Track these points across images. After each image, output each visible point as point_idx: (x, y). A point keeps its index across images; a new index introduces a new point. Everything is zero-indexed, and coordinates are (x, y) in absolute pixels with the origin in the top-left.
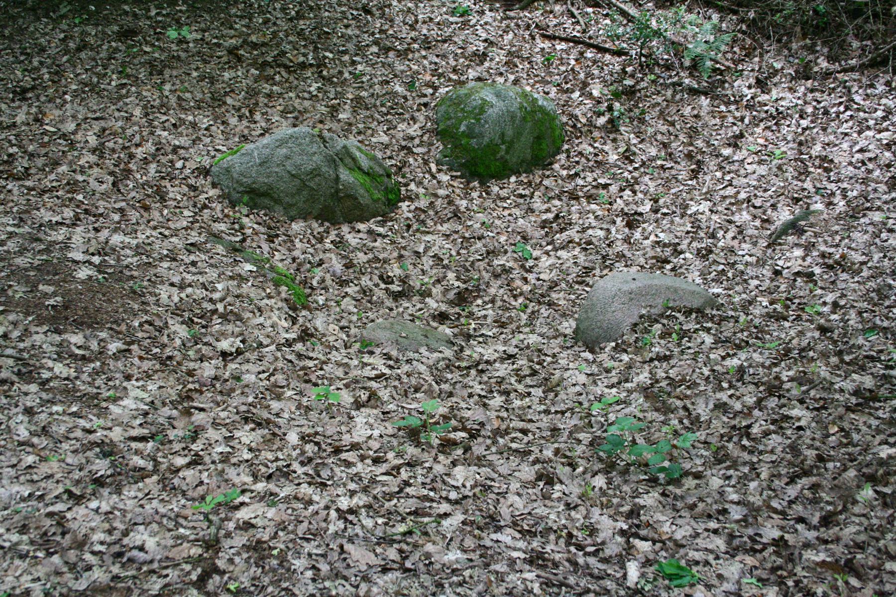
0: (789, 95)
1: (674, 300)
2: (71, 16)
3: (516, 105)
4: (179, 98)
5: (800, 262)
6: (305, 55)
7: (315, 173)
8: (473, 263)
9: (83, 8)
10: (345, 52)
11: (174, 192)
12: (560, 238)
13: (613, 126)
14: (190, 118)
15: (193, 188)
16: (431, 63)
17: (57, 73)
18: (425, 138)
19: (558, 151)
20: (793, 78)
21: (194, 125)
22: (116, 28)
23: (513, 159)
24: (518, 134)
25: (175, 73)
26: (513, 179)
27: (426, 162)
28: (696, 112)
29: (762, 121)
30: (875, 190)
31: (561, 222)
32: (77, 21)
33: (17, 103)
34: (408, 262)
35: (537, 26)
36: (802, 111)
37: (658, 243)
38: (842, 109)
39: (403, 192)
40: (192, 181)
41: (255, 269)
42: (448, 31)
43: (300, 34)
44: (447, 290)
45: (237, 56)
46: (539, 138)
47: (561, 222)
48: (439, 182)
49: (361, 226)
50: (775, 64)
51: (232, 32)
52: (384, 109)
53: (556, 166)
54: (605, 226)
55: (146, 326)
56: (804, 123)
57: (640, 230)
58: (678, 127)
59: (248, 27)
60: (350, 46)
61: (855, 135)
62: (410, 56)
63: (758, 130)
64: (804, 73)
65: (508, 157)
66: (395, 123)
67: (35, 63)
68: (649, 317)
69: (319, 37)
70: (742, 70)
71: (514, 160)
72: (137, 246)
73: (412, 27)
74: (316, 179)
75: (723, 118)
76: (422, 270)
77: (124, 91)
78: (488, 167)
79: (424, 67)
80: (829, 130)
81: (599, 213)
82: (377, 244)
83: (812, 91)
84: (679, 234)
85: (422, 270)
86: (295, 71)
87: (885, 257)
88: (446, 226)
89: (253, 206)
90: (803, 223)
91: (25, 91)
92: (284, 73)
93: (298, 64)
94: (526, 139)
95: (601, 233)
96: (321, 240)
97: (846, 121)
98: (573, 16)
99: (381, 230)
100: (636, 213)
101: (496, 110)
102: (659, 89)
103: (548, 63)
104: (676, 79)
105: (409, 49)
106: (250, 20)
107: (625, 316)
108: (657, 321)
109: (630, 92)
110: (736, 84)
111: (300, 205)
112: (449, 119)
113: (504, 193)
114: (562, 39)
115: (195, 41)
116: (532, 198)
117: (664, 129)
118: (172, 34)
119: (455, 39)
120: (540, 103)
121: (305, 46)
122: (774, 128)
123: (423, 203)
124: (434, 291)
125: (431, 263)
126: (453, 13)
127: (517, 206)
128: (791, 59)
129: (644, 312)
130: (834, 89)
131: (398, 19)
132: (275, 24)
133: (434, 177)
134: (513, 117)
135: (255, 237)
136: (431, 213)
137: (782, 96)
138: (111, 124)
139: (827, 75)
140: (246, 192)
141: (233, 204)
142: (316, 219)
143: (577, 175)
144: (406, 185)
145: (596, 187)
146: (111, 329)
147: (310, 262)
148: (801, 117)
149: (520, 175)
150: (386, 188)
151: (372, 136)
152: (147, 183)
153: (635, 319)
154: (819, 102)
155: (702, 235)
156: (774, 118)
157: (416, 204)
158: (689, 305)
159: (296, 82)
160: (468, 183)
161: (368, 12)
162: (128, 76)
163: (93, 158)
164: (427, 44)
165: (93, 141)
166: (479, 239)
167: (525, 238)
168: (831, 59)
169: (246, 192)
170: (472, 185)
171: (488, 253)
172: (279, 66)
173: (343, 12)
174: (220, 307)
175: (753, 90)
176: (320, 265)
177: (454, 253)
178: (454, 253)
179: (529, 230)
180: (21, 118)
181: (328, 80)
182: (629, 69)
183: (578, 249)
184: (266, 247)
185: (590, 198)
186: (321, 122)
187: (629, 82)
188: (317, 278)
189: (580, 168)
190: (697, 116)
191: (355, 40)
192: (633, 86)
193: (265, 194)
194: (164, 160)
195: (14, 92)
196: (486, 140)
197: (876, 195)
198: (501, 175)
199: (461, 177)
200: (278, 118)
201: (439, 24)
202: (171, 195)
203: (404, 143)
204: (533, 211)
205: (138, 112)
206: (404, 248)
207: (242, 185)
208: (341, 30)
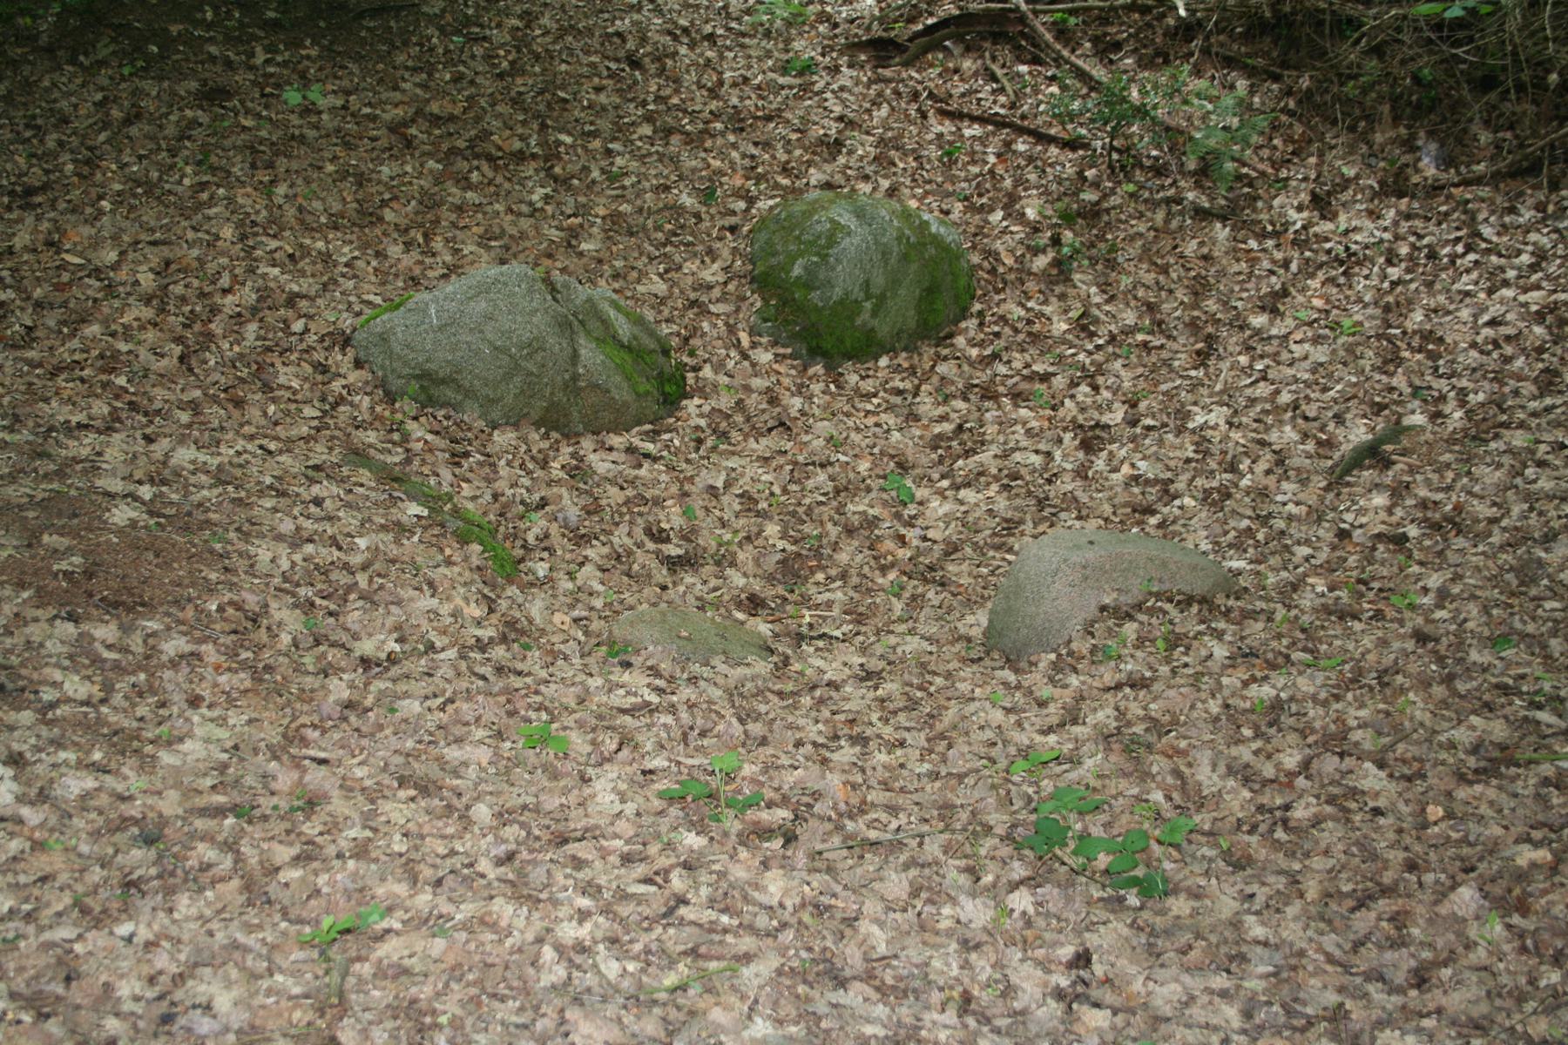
0: (1368, 224)
3: (892, 233)
6: (522, 138)
7: (534, 347)
8: (810, 508)
10: (594, 134)
11: (287, 376)
14: (320, 245)
17: (88, 162)
18: (731, 287)
19: (964, 314)
20: (1375, 195)
22: (193, 85)
23: (883, 329)
24: (894, 282)
25: (295, 165)
26: (884, 361)
27: (731, 329)
28: (1205, 250)
29: (1320, 266)
32: (126, 71)
35: (931, 95)
38: (1460, 249)
40: (319, 356)
42: (776, 102)
45: (404, 136)
46: (931, 291)
49: (616, 440)
50: (1345, 170)
53: (960, 341)
54: (1042, 447)
56: (1394, 273)
58: (1174, 275)
59: (424, 86)
60: (604, 124)
61: (1482, 295)
62: (709, 144)
63: (1314, 284)
64: (1395, 186)
70: (1287, 179)
72: (220, 467)
75: (1253, 262)
79: (732, 163)
80: (1438, 286)
81: (1034, 424)
84: (1172, 464)
87: (1531, 509)
88: (764, 441)
90: (1389, 448)
91: (30, 191)
92: (485, 167)
95: (1036, 460)
97: (1468, 271)
98: (994, 78)
101: (856, 240)
102: (1142, 208)
103: (949, 160)
104: (1172, 191)
105: (706, 131)
109: (1093, 214)
110: (1276, 203)
113: (868, 386)
114: (973, 119)
117: (1149, 278)
119: (788, 115)
120: (933, 229)
121: (524, 123)
122: (1342, 280)
123: (725, 402)
125: (738, 508)
126: (784, 71)
129: (1107, 600)
130: (1446, 214)
132: (472, 82)
136: (739, 418)
137: (1357, 225)
139: (1436, 189)
140: (418, 377)
142: (537, 425)
143: (995, 356)
144: (696, 369)
145: (1029, 378)
148: (1389, 262)
150: (661, 374)
156: (1342, 263)
158: (1187, 589)
161: (635, 64)
163: (148, 313)
164: (738, 122)
165: (147, 280)
166: (822, 466)
167: (903, 467)
169: (418, 377)
170: (811, 371)
171: (838, 491)
172: (477, 156)
173: (593, 65)
175: (1305, 214)
177: (777, 490)
178: (777, 490)
185: (1017, 397)
186: (550, 256)
187: (1089, 196)
192: (1098, 203)
194: (270, 317)
196: (838, 292)
197: (1518, 401)
198: (866, 349)
199: (792, 357)
201: (759, 87)
203: (693, 296)
205: (228, 232)
207: (406, 364)
208: (588, 97)
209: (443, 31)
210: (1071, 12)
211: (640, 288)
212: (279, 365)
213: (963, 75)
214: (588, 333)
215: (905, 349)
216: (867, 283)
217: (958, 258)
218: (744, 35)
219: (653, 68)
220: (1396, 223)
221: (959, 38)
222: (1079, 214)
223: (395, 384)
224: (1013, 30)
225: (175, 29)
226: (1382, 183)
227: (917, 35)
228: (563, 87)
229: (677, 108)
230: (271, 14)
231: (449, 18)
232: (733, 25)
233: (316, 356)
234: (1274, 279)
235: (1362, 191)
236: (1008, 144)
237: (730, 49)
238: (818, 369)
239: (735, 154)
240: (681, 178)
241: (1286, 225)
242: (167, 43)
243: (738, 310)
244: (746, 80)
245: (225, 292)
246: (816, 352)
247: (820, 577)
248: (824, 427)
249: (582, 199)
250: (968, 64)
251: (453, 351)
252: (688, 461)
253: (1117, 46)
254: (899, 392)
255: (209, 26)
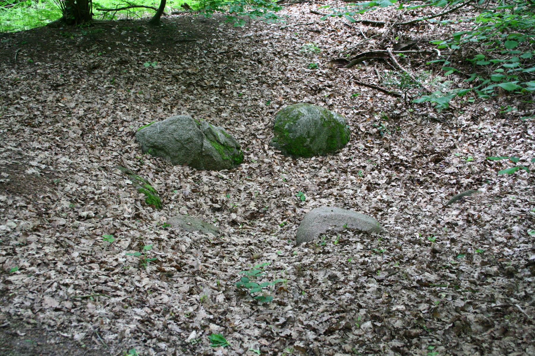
0: (489, 127)
1: (352, 225)
2: (97, 51)
3: (319, 116)
4: (136, 97)
5: (454, 217)
6: (215, 81)
7: (189, 140)
8: (269, 198)
9: (105, 48)
10: (238, 82)
11: (112, 142)
12: (326, 192)
13: (380, 135)
14: (138, 107)
15: (124, 142)
16: (285, 92)
17: (78, 79)
18: (266, 131)
19: (344, 146)
20: (494, 117)
21: (138, 111)
22: (118, 59)
23: (314, 147)
24: (319, 133)
25: (139, 84)
26: (313, 158)
27: (263, 143)
28: (431, 132)
29: (469, 139)
30: (519, 184)
31: (330, 183)
32: (99, 54)
33: (52, 91)
34: (231, 195)
35: (354, 77)
36: (494, 136)
37: (380, 200)
38: (518, 137)
39: (246, 158)
40: (124, 138)
41: (131, 183)
42: (302, 76)
43: (217, 71)
44: (246, 211)
45: (176, 78)
46: (332, 137)
47: (330, 183)
48: (267, 155)
49: (214, 173)
50: (486, 109)
51: (180, 66)
52: (249, 114)
53: (341, 154)
54: (355, 189)
55: (47, 199)
56: (494, 143)
57: (374, 192)
58: (418, 139)
59: (189, 64)
60: (243, 80)
61: (522, 152)
62: (274, 88)
63: (466, 145)
64: (500, 116)
65: (311, 146)
66: (252, 121)
67: (70, 73)
68: (332, 232)
69: (227, 73)
70: (465, 110)
71: (315, 148)
72: (71, 164)
73: (283, 73)
74: (190, 144)
75: (446, 136)
76: (238, 199)
77: (109, 91)
78: (298, 150)
79: (281, 94)
80: (508, 148)
81: (355, 181)
82: (218, 183)
83: (504, 125)
84: (395, 197)
85: (238, 199)
86: (206, 89)
87: (503, 219)
88: (263, 178)
89: (154, 155)
90: (466, 197)
91: (58, 85)
92: (199, 90)
93: (210, 86)
94: (323, 137)
95: (351, 192)
96: (186, 177)
97: (519, 144)
98: (376, 74)
99: (225, 176)
100: (376, 184)
101: (305, 118)
102: (414, 117)
103: (353, 98)
104: (425, 112)
105: (274, 84)
106: (193, 61)
107: (316, 229)
108: (336, 234)
109: (397, 118)
110: (459, 118)
111: (181, 157)
112: (281, 121)
113: (305, 165)
114: (366, 86)
115: (158, 69)
116: (320, 169)
117: (409, 139)
118: (147, 65)
119: (304, 81)
120: (334, 117)
121: (217, 77)
122: (475, 144)
123: (254, 165)
124: (240, 210)
125: (246, 196)
126: (308, 67)
127: (309, 172)
128: (496, 107)
129: (330, 228)
130: (517, 125)
131: (275, 68)
132: (205, 64)
133: (265, 152)
134: (316, 123)
135: (148, 171)
136: (258, 171)
137: (486, 127)
138: (94, 106)
139: (516, 117)
140: (152, 147)
141: (143, 153)
142: (189, 165)
143: (350, 159)
144: (248, 154)
145: (359, 167)
146: (25, 196)
147: (174, 187)
148: (493, 140)
149: (318, 156)
150: (234, 155)
151: (237, 126)
152: (100, 137)
153: (323, 231)
154: (506, 132)
155: (409, 199)
156: (476, 139)
157: (251, 165)
158: (360, 228)
159: (205, 95)
160: (286, 157)
161: (260, 62)
162: (115, 83)
163: (77, 121)
164: (287, 82)
165: (81, 113)
166: (279, 187)
167: (306, 190)
168: (520, 108)
169: (152, 147)
170: (287, 159)
171: (281, 194)
172: (198, 86)
173: (246, 62)
174: (96, 197)
175: (468, 122)
176: (179, 189)
177: (261, 193)
178: (261, 193)
179: (309, 186)
180: (50, 98)
181: (224, 96)
182: (399, 105)
183: (333, 199)
184: (151, 176)
185: (353, 173)
186: (209, 116)
187: (397, 112)
188: (175, 195)
189: (353, 156)
190: (431, 134)
191: (246, 77)
192: (399, 114)
193: (161, 149)
194: (114, 126)
195: (52, 86)
196: (298, 134)
197: (519, 186)
198: (307, 154)
199: (281, 153)
200: (184, 112)
201: (298, 72)
202: (110, 144)
203: (253, 132)
204: (317, 176)
205: (111, 101)
206: (233, 187)
207: (149, 143)
208: (241, 70)
209: (201, 49)
210: (405, 53)
211: (237, 129)
212: (111, 140)
213: (370, 73)
214: (208, 138)
215: (322, 155)
216: (309, 132)
217: (343, 127)
218: (298, 55)
219: (265, 64)
220: (499, 127)
221: (368, 60)
222: (392, 118)
223: (145, 148)
224: (386, 58)
225: (117, 43)
226: (497, 114)
227: (354, 58)
228: (234, 67)
229: (268, 76)
230: (148, 40)
231: (204, 45)
232: (295, 52)
233: (123, 138)
234: (452, 142)
235: (490, 116)
236: (375, 94)
237: (292, 59)
238: (290, 158)
239: (282, 91)
240: (262, 97)
241: (461, 125)
242: (114, 46)
243: (266, 138)
244: (294, 69)
245: (104, 118)
246: (289, 153)
247: (262, 219)
248: (285, 176)
249: (227, 101)
250: (369, 69)
251: (163, 140)
252: (236, 181)
253: (418, 65)
254: (314, 168)
255: (128, 43)
